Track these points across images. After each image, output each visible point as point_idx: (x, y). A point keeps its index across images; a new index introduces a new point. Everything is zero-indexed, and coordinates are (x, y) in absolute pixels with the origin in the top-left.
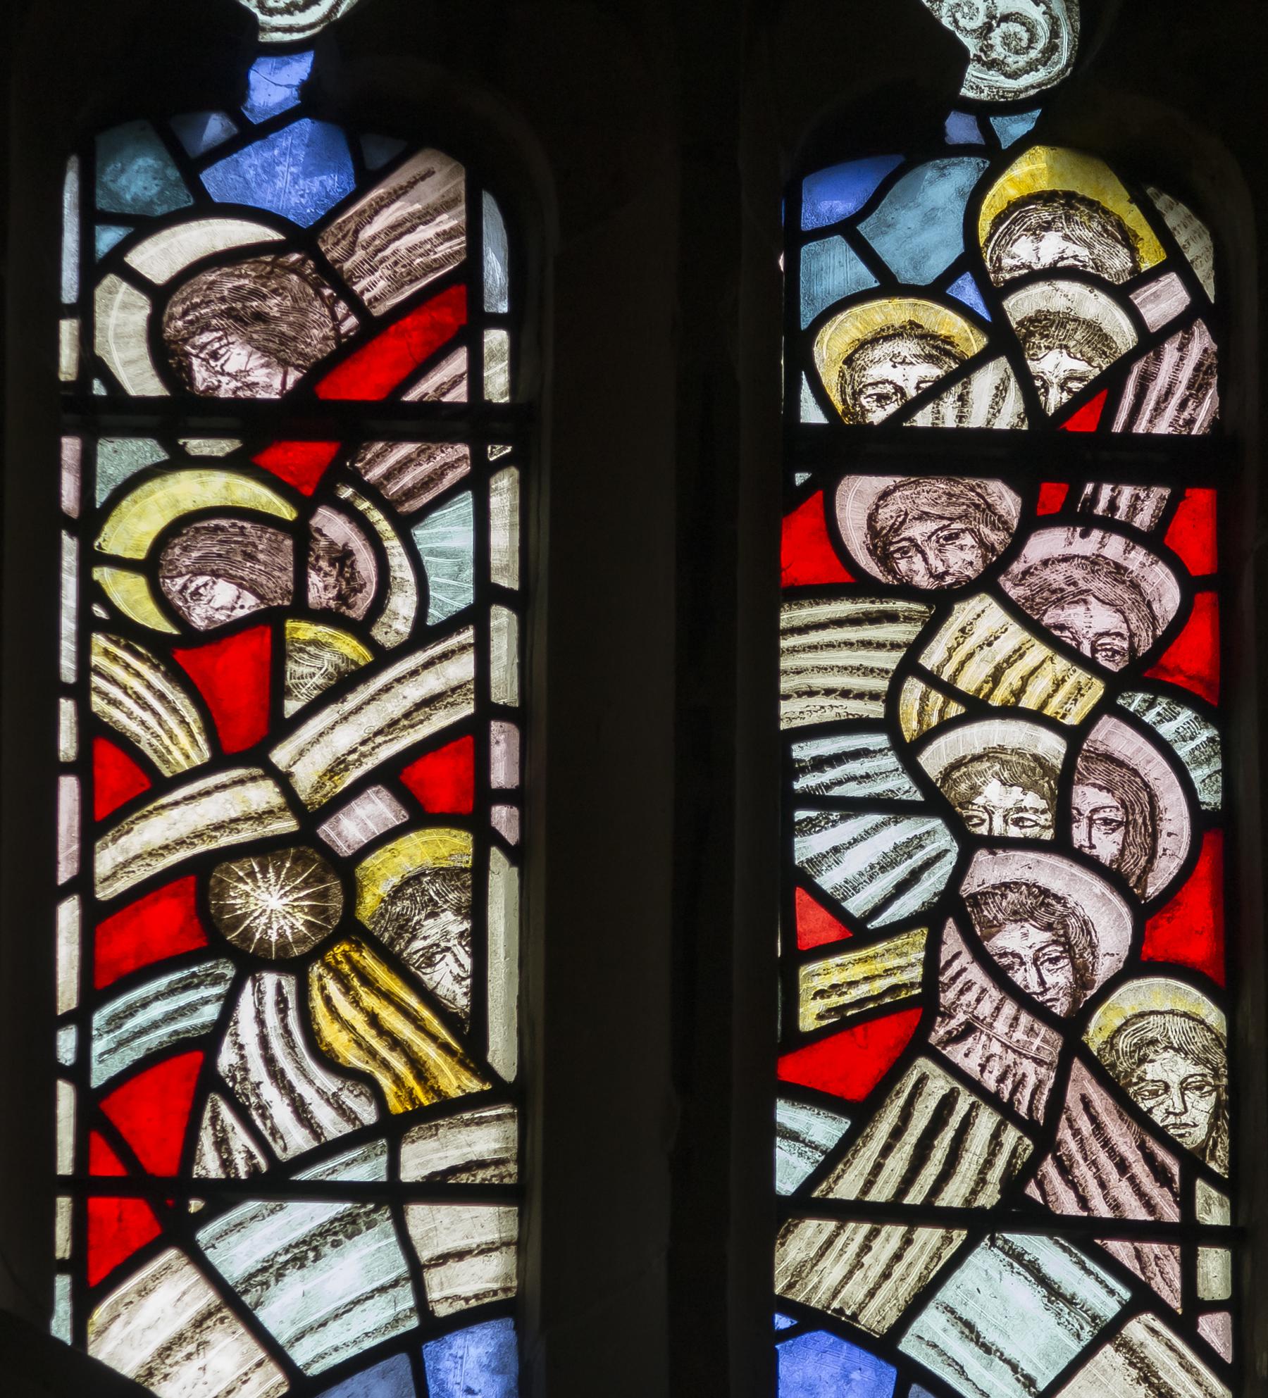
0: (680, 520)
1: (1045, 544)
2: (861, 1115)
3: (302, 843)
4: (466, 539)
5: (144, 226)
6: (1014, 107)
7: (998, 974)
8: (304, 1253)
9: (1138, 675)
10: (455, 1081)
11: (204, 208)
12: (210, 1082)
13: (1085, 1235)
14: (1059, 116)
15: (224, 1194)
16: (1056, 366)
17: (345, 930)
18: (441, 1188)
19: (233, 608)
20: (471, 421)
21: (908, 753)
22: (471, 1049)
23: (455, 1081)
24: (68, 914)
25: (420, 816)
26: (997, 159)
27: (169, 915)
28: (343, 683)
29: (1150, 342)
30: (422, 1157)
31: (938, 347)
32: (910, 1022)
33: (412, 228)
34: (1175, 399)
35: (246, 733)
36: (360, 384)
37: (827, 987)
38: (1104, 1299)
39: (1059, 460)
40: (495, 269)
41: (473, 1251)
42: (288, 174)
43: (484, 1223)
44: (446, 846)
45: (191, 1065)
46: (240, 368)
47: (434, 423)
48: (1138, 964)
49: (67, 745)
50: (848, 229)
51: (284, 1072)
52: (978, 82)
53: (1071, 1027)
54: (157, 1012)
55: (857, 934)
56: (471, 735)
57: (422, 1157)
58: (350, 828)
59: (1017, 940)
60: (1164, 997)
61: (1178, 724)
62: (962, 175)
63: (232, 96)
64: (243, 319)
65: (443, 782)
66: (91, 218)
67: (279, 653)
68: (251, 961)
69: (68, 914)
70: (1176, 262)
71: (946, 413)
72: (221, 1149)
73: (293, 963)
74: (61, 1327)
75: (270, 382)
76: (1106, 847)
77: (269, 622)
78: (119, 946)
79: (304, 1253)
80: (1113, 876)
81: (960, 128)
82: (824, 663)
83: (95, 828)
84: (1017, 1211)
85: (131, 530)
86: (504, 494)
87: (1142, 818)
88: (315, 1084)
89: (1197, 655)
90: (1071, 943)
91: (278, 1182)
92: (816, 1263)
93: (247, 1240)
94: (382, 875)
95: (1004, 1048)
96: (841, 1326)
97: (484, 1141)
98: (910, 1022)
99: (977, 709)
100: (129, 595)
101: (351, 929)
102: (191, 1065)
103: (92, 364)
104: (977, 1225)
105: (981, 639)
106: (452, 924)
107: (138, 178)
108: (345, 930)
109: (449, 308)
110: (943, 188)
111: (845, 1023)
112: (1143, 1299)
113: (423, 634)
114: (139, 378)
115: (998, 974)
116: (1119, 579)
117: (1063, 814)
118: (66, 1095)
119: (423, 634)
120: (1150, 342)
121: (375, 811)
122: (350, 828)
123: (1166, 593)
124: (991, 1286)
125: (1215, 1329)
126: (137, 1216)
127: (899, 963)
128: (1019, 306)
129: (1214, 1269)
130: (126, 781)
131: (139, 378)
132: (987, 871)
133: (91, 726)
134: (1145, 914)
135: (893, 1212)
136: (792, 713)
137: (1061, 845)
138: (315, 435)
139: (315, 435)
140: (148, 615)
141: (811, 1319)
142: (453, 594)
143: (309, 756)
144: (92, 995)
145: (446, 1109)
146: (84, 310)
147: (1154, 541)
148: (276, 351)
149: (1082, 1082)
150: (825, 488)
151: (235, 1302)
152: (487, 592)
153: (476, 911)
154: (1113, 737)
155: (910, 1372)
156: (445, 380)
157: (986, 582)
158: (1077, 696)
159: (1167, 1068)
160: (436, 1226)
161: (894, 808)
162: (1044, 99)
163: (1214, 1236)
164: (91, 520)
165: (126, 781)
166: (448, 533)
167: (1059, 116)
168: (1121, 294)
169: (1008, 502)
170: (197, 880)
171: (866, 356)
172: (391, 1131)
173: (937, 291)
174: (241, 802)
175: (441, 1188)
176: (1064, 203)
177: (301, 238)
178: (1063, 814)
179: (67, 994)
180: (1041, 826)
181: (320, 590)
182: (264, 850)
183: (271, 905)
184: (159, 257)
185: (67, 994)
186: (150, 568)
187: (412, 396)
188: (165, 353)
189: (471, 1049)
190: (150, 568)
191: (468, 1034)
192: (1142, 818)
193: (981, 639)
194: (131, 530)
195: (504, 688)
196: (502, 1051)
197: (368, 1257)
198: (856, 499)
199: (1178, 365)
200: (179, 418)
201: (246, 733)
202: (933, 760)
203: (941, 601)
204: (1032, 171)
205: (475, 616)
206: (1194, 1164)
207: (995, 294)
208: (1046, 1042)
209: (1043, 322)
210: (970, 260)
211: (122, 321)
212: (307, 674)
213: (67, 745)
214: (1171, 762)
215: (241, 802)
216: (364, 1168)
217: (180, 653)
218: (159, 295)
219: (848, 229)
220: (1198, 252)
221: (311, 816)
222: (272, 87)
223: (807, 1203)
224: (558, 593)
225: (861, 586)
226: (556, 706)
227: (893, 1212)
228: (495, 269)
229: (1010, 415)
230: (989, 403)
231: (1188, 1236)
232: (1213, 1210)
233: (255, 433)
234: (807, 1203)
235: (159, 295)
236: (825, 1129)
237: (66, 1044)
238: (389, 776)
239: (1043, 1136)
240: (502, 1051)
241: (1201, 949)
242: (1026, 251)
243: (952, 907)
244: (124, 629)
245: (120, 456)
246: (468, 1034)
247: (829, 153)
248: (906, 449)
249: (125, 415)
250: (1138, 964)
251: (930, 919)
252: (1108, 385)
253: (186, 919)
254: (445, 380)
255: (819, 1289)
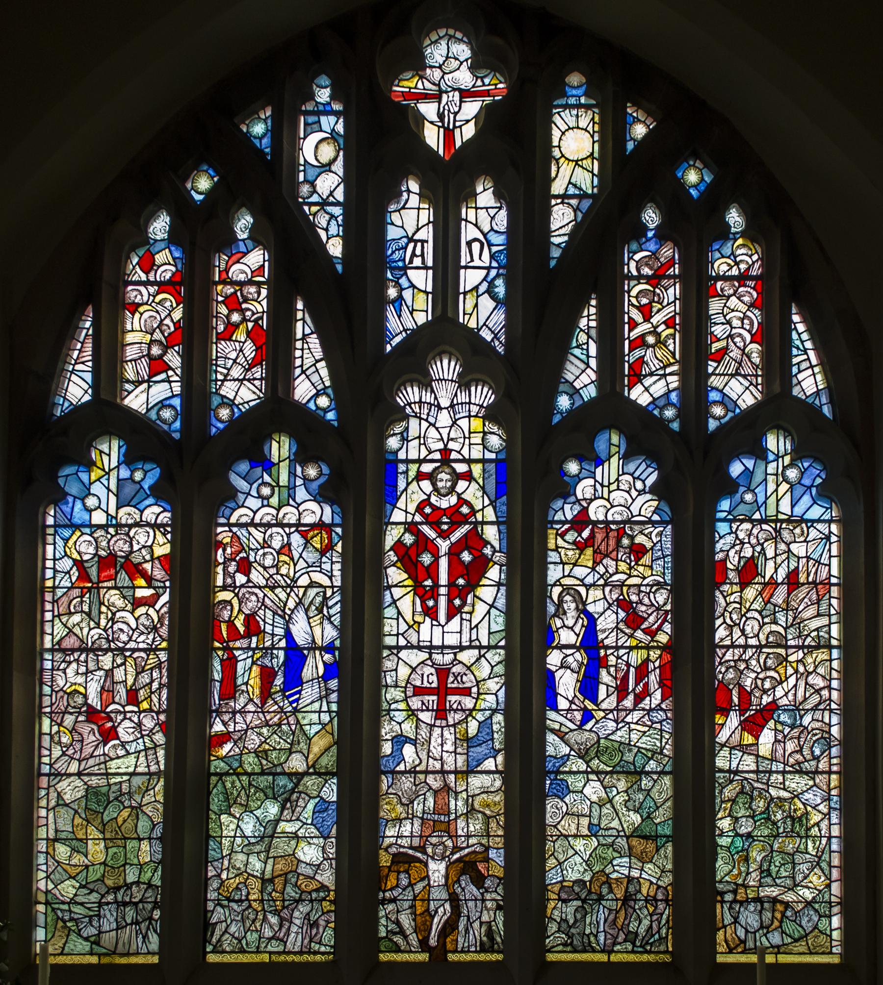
0: (699, 288)
1: (741, 289)
2: (719, 362)
3: (654, 332)
4: (673, 292)
5: (635, 253)
6: (737, 233)
7: (735, 344)
8: (655, 383)
9: (752, 305)
10: (672, 361)
11: (642, 250)
12: (644, 362)
13: (745, 376)
14: (743, 234)
15: (645, 376)
16: (743, 266)
17: (660, 343)
18: (671, 374)
19: (108, 489)
20: (674, 277)
21: (725, 317)
22: (674, 357)
23: (672, 361)
24: (627, 342)
25: (668, 327)
26: (736, 240)
27: (639, 341)
28: (659, 311)
29: (753, 263)
30: (668, 370)
31: (729, 265)
32: (724, 351)
33: (667, 252)
34: (756, 271)
35: (647, 318)
36: (660, 273)
37: (716, 346)
38: (747, 384)
39: (742, 278)
40: (677, 256)
41: (674, 381)
42: (652, 246)
43: (676, 378)
44: (671, 331)
45: (641, 361)
46: (646, 271)
47: (669, 277)
48: (751, 342)
49: (626, 320)
50: (718, 250)
51: (652, 359)
52: (733, 230)
53: (743, 350)
54: (638, 353)
55: (718, 340)
56: (674, 317)
57: (668, 370)
58: (659, 330)
59: (737, 340)
60: (755, 347)
61: (756, 312)
62: (731, 242)
63: (645, 235)
64: (647, 265)
65: (670, 322)
66: (629, 252)
67: (652, 307)
68: (648, 346)
69: (627, 342)
70: (757, 252)
71: (729, 273)
72: (645, 370)
73: (653, 346)
74: (626, 394)
75: (650, 273)
76: (748, 327)
77: (650, 303)
78: (633, 345)
79: (655, 383)
80: (749, 331)
81: (731, 236)
82: (715, 306)
83: (630, 331)
84: (737, 374)
85: (634, 292)
86: (678, 286)
87: (752, 324)
88: (656, 362)
89: (759, 303)
90: (744, 340)
91: (652, 374)
92: (714, 381)
93: (648, 382)
94: (664, 335)
95: (735, 353)
96: (717, 389)
97: (675, 368)
98: (724, 351)
99: (733, 311)
100: (634, 301)
101: (660, 342)
102: (641, 361)
103: (629, 271)
104: (732, 376)
105: (733, 302)
106: (671, 341)
107: (634, 246)
108: (660, 343)
109: (671, 263)
110: (730, 244)
111: (717, 351)
112: (751, 384)
113: (668, 304)
114: (635, 273)
115: (735, 344)
116: (749, 293)
117: (743, 323)
118: (626, 365)
119: (668, 304)
120: (753, 263)
121: (663, 327)
122: (659, 330)
123: (755, 295)
124: (734, 383)
125: (760, 387)
126: (635, 378)
127: (723, 344)
128: (738, 259)
129: (760, 379)
130: (633, 324)
131: (635, 273)
132: (734, 331)
133: (629, 318)
134: (752, 336)
135: (723, 374)
136: (711, 312)
137: (742, 328)
138: (655, 280)
139: (655, 280)
140: (636, 303)
141: (713, 388)
142: (672, 299)
143: (654, 320)
144: (630, 351)
145: (671, 364)
146: (628, 264)
147: (754, 288)
148: (651, 269)
149: (745, 357)
150: (715, 284)
151: (647, 389)
152: (676, 299)
153: (674, 339)
154: (749, 313)
155: (725, 394)
156: (670, 272)
157: (734, 294)
158: (744, 308)
159: (754, 355)
160: (670, 379)
161: (723, 324)
162: (741, 232)
163: (835, 773)
164: (629, 292)
165: (633, 324)
166: (671, 291)
167: (743, 234)
168: (750, 256)
169: (737, 284)
170: (642, 337)
171: (721, 266)
172: (665, 367)
173: (729, 257)
174: (646, 327)
175: (671, 374)
176: (743, 246)
177: (654, 253)
178: (743, 323)
179: (627, 351)
180: (740, 325)
181: (656, 299)
182: (650, 333)
183: (651, 340)
184: (637, 257)
185: (627, 351)
186: (637, 297)
187: (90, 311)
188: (638, 269)
189: (674, 357)
190: (637, 297)
191: (673, 354)
192: (752, 324)
193: (733, 302)
194: (634, 292)
195: (678, 311)
196: (677, 357)
197: (662, 382)
198: (719, 285)
199: (756, 266)
200: (639, 278)
201: (647, 318)
202: (728, 318)
203: (729, 297)
204: (740, 241)
205: (674, 302)
206: (757, 367)
207: (735, 257)
208: (740, 352)
209: (741, 261)
210: (732, 253)
211: (633, 265)
212: (655, 310)
213: (626, 320)
214: (756, 316)
215: (646, 327)
216: (662, 372)
217: (640, 308)
218: (637, 262)
219: (718, 250)
220: (759, 251)
221: (655, 327)
222: (650, 234)
223: (713, 374)
224: (684, 298)
225: (719, 296)
226: (684, 313)
227: (723, 374)
228: (677, 256)
229: (737, 273)
230: (735, 272)
231: (757, 376)
232: (760, 373)
233: (649, 279)
234: (713, 374)
235: (637, 262)
236: (715, 365)
237: (626, 358)
238: (664, 322)
239: (740, 364)
240: (677, 357)
241: (759, 340)
242: (739, 252)
243: (731, 336)
244: (633, 305)
245: (633, 283)
246: (673, 354)
247: (716, 239)
248: (725, 278)
249: (632, 278)
250: (751, 342)
251: (727, 338)
252: (748, 269)
253: (640, 343)
254: (670, 272)
255: (714, 385)
